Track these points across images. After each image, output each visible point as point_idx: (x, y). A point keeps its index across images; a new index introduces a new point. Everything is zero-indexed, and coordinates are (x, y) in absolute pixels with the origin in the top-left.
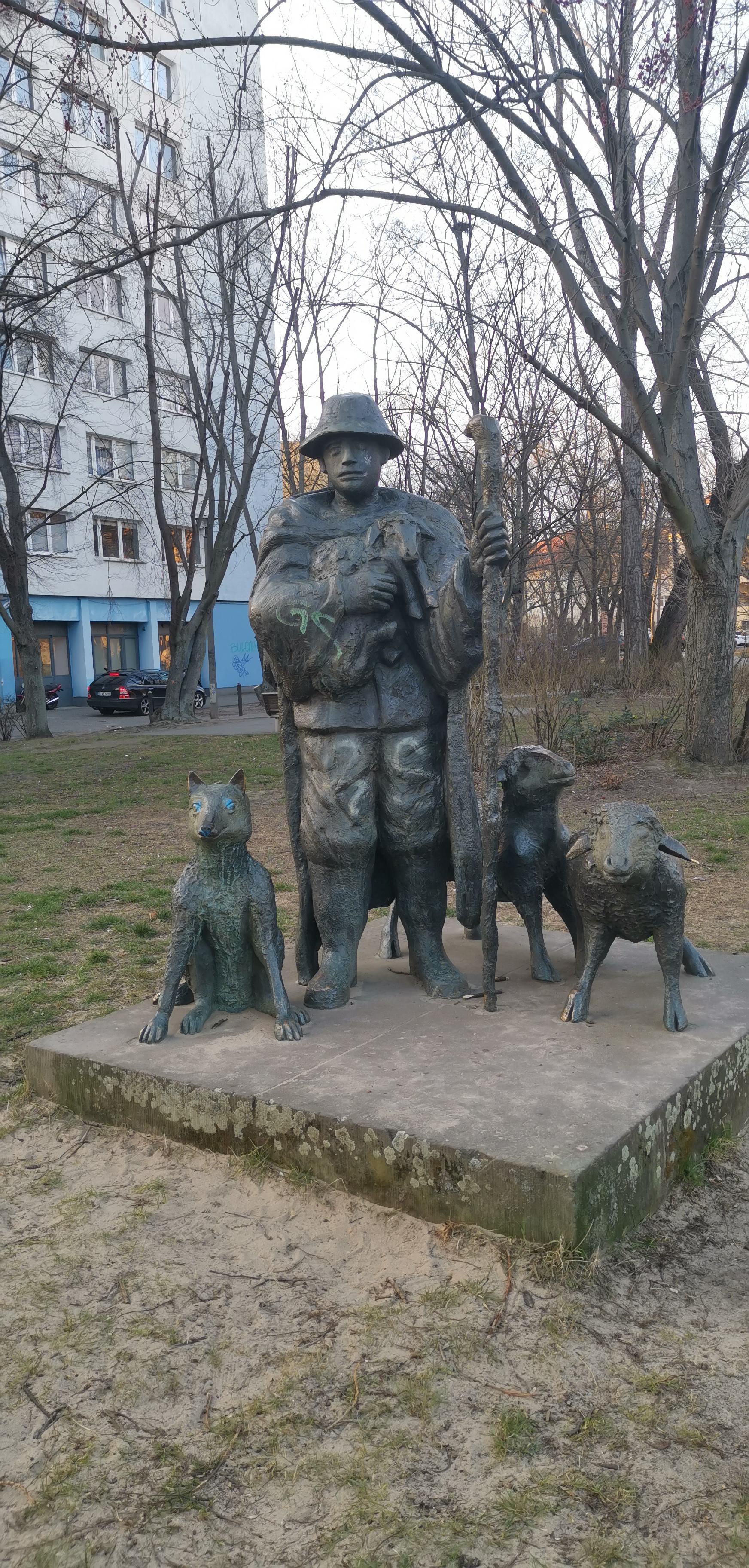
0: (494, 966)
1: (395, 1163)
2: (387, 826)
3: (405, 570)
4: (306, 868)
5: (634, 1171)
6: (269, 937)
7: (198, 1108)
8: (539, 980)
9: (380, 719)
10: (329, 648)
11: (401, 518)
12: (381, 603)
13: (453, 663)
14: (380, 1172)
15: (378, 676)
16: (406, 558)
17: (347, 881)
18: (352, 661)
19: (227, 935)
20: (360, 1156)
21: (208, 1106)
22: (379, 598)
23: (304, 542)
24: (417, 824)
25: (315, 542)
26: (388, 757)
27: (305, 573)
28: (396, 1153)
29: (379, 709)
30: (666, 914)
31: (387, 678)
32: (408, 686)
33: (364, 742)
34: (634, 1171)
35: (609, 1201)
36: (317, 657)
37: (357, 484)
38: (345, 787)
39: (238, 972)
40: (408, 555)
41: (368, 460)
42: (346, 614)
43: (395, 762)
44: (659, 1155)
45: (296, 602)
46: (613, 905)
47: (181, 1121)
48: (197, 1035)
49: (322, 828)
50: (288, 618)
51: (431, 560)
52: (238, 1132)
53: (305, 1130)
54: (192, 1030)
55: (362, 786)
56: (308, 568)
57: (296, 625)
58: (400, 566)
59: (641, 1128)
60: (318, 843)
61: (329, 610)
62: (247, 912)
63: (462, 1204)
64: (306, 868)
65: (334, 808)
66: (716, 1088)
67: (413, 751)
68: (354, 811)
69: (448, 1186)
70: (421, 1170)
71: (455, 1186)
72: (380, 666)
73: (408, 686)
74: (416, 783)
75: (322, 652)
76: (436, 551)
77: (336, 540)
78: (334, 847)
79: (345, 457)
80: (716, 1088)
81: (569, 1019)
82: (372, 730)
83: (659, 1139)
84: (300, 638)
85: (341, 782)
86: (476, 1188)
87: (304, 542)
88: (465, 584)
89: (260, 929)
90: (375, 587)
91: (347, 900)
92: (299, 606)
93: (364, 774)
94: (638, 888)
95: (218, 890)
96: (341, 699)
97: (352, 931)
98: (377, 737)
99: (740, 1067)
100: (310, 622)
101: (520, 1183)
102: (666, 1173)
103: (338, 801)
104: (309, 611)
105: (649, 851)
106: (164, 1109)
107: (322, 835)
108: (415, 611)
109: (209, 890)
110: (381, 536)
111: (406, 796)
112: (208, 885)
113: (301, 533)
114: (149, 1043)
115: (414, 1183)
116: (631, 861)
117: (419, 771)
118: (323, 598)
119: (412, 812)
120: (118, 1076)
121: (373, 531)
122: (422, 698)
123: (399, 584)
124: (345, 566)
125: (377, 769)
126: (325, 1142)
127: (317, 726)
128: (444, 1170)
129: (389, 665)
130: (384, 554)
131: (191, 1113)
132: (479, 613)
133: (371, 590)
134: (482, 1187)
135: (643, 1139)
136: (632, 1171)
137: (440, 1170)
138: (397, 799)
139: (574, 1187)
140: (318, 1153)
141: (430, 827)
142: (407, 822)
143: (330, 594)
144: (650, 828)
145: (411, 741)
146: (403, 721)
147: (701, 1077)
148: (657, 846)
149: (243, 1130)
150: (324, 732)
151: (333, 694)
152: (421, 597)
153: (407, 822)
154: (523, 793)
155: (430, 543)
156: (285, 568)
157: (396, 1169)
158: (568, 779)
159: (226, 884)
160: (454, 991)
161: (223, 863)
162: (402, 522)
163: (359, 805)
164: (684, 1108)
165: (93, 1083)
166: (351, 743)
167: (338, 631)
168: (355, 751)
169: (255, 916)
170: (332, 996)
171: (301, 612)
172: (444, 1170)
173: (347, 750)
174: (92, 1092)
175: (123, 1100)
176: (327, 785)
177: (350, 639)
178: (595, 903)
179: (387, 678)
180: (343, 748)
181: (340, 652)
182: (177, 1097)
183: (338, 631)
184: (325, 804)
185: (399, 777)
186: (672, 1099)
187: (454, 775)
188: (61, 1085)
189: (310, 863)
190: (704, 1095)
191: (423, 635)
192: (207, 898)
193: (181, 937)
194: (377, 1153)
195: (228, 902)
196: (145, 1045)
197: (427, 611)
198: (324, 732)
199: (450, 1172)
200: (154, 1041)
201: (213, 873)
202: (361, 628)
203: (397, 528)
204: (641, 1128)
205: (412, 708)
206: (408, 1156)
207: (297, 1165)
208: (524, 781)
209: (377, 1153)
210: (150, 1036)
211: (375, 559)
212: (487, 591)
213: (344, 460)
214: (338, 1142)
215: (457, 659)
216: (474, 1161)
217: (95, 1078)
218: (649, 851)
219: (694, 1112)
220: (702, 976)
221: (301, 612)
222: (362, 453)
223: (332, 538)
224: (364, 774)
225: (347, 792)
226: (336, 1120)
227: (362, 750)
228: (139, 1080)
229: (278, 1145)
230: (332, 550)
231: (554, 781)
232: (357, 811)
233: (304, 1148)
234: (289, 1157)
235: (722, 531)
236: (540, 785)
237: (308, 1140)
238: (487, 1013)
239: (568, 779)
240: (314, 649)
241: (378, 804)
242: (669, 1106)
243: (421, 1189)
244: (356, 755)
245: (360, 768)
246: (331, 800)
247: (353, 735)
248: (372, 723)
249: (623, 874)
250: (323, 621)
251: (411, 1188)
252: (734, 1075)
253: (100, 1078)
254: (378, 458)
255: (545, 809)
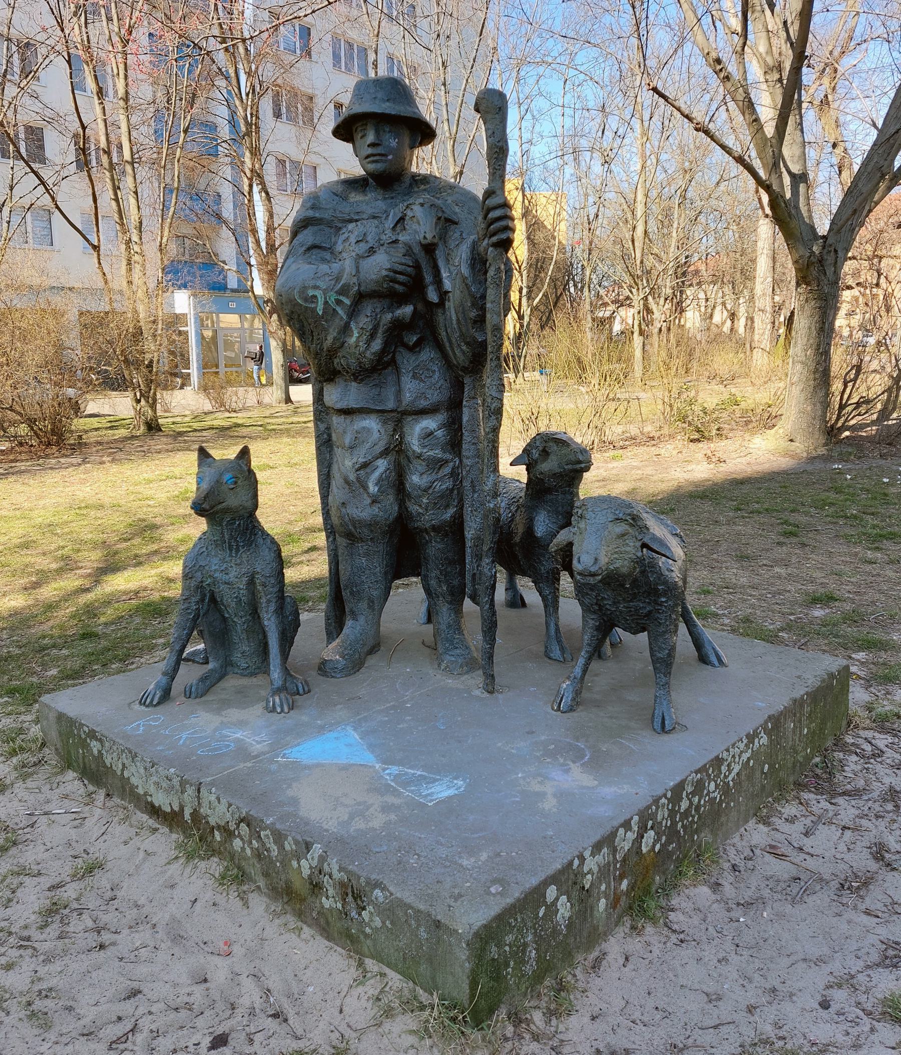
0: (492, 648)
1: (310, 877)
2: (408, 504)
3: (423, 254)
4: (335, 539)
5: (564, 909)
6: (272, 607)
7: (157, 784)
8: (550, 658)
9: (399, 400)
10: (346, 329)
11: (421, 201)
12: (397, 286)
13: (464, 348)
14: (297, 884)
15: (398, 358)
16: (424, 242)
17: (367, 554)
18: (368, 343)
19: (233, 604)
20: (281, 863)
21: (164, 785)
22: (394, 281)
23: (329, 224)
24: (435, 504)
25: (340, 225)
26: (408, 438)
27: (327, 256)
28: (311, 868)
29: (399, 392)
30: (658, 611)
31: (407, 362)
32: (428, 369)
33: (385, 423)
34: (564, 909)
35: (524, 952)
36: (335, 338)
37: (379, 167)
38: (365, 465)
39: (248, 639)
40: (425, 238)
41: (394, 143)
42: (361, 297)
43: (414, 444)
44: (603, 887)
45: (312, 283)
46: (603, 598)
47: (146, 794)
48: (198, 700)
49: (343, 503)
50: (306, 300)
51: (452, 244)
52: (187, 817)
53: (238, 825)
54: (193, 695)
55: (382, 465)
56: (330, 249)
57: (313, 306)
58: (417, 249)
59: (576, 862)
60: (341, 517)
61: (343, 291)
62: (251, 582)
63: (367, 936)
64: (335, 539)
65: (357, 485)
66: (691, 803)
67: (431, 433)
68: (373, 488)
69: (354, 914)
70: (331, 892)
71: (360, 915)
72: (401, 349)
73: (428, 369)
74: (435, 464)
75: (339, 333)
76: (457, 235)
77: (358, 223)
78: (353, 522)
79: (371, 137)
80: (691, 803)
81: (559, 709)
82: (392, 411)
83: (604, 872)
84: (317, 319)
85: (361, 460)
86: (378, 922)
87: (329, 224)
88: (472, 266)
89: (264, 600)
90: (390, 270)
91: (367, 572)
92: (316, 287)
93: (385, 453)
94: (623, 585)
95: (223, 561)
96: (362, 380)
97: (373, 602)
98: (397, 419)
99: (726, 777)
100: (326, 303)
101: (417, 928)
102: (614, 903)
103: (358, 479)
104: (325, 292)
105: (628, 549)
106: (134, 781)
107: (343, 510)
108: (433, 296)
109: (215, 561)
110: (402, 219)
111: (425, 476)
112: (216, 556)
113: (326, 216)
114: (147, 706)
115: (327, 903)
116: (603, 560)
117: (437, 453)
118: (338, 279)
119: (430, 491)
120: (100, 741)
121: (395, 214)
122: (442, 381)
123: (417, 267)
124: (363, 247)
125: (396, 450)
126: (254, 842)
127: (339, 406)
128: (350, 896)
129: (412, 349)
130: (402, 238)
131: (152, 789)
132: (483, 297)
133: (384, 273)
134: (384, 923)
135: (580, 873)
136: (561, 911)
137: (347, 895)
138: (416, 479)
139: (468, 945)
140: (248, 852)
141: (447, 506)
142: (425, 501)
143: (345, 276)
144: (631, 525)
145: (429, 423)
146: (423, 404)
147: (669, 795)
148: (639, 544)
149: (191, 814)
150: (347, 412)
151: (353, 375)
152: (438, 281)
153: (425, 501)
154: (542, 477)
155: (453, 227)
156: (309, 249)
157: (311, 883)
158: (583, 465)
159: (231, 556)
160: (461, 666)
161: (227, 537)
162: (422, 205)
163: (379, 482)
164: (643, 829)
165: (84, 745)
166: (371, 423)
167: (353, 312)
168: (376, 431)
169: (259, 588)
170: (340, 666)
171: (317, 293)
172: (350, 896)
173: (368, 430)
174: (84, 753)
175: (105, 766)
176: (348, 463)
177: (364, 320)
178: (587, 594)
179: (407, 362)
180: (364, 428)
181: (356, 335)
182: (142, 771)
183: (353, 312)
184: (347, 481)
185: (419, 457)
186: (627, 825)
187: (467, 458)
188: (62, 741)
189: (337, 535)
190: (672, 813)
191: (440, 319)
192: (214, 568)
193: (186, 605)
194: (295, 864)
195: (233, 574)
196: (143, 708)
197: (443, 295)
198: (347, 412)
199: (355, 899)
200: (151, 704)
201: (219, 544)
202: (378, 310)
203: (417, 209)
204: (576, 862)
205: (431, 392)
206: (320, 873)
207: (232, 858)
208: (543, 465)
209: (295, 864)
210: (148, 700)
211: (394, 242)
212: (491, 273)
213: (368, 143)
214: (264, 844)
215: (467, 344)
216: (377, 892)
217: (85, 740)
218: (628, 549)
219: (657, 833)
220: (713, 665)
221: (317, 293)
222: (388, 136)
223: (357, 221)
224: (385, 453)
225: (368, 470)
226: (262, 821)
227: (382, 431)
228: (115, 748)
229: (218, 836)
230: (353, 231)
231: (570, 467)
232: (376, 489)
233: (237, 843)
234: (225, 849)
235: (825, 242)
236: (558, 470)
237: (240, 836)
238: (486, 695)
239: (583, 465)
240: (331, 330)
241: (398, 483)
242: (621, 831)
243: (331, 910)
244: (376, 435)
245: (380, 448)
246: (352, 477)
247: (373, 416)
248: (390, 405)
249: (593, 575)
250: (339, 302)
251: (323, 907)
252: (717, 786)
253: (88, 741)
254: (407, 141)
255: (564, 493)
